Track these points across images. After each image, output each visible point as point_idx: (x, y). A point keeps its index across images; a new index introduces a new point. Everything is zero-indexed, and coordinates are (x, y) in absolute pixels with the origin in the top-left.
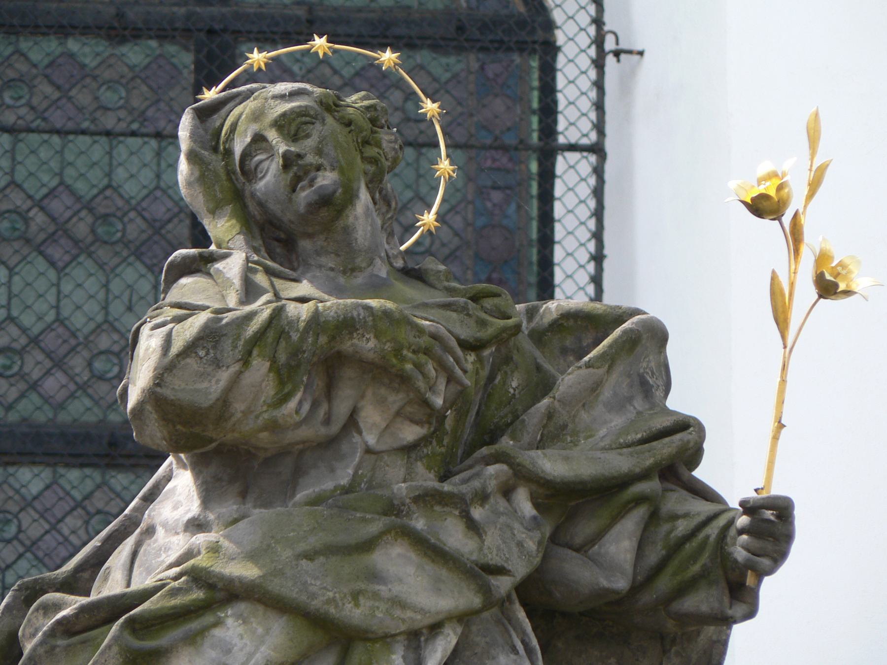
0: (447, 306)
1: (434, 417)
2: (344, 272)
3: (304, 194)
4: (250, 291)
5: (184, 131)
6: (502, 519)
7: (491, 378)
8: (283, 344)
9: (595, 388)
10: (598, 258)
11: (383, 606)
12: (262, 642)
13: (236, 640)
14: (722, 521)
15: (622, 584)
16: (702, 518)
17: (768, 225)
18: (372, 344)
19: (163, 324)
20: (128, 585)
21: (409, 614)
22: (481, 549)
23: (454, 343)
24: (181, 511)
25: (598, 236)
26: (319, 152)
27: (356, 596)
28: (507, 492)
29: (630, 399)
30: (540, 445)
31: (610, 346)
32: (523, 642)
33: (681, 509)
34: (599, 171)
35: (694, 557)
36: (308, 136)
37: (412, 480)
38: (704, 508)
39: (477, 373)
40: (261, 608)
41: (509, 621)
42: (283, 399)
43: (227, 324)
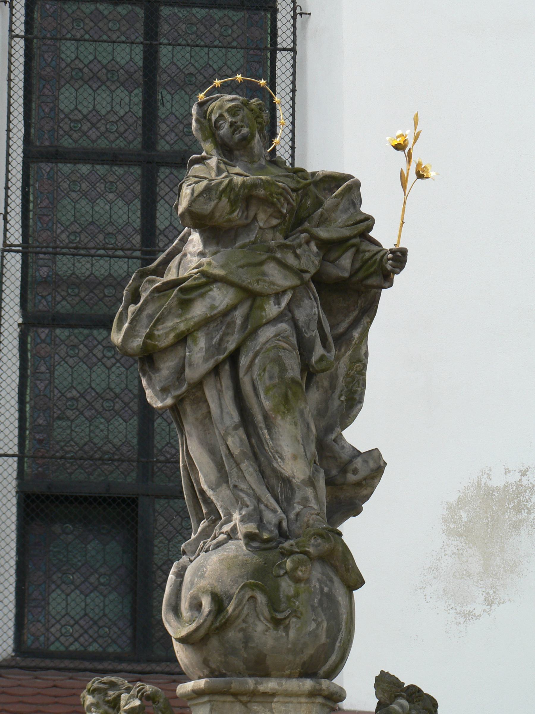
0: (286, 176)
1: (282, 216)
2: (250, 163)
3: (237, 136)
4: (219, 171)
5: (194, 110)
6: (307, 253)
7: (301, 201)
8: (233, 193)
9: (337, 205)
10: (294, 91)
11: (267, 285)
12: (226, 297)
13: (217, 296)
14: (381, 254)
15: (346, 275)
16: (374, 252)
17: (401, 153)
18: (263, 192)
19: (191, 185)
20: (178, 275)
21: (276, 287)
22: (300, 264)
23: (290, 190)
24: (196, 248)
25: (293, 82)
26: (242, 121)
27: (258, 281)
28: (308, 243)
29: (349, 209)
30: (318, 226)
31: (342, 190)
32: (313, 295)
33: (367, 248)
34: (294, 58)
35: (372, 266)
36: (238, 115)
37: (275, 240)
38: (375, 248)
39: (297, 200)
40: (225, 285)
41: (308, 288)
42: (233, 212)
43: (214, 185)
